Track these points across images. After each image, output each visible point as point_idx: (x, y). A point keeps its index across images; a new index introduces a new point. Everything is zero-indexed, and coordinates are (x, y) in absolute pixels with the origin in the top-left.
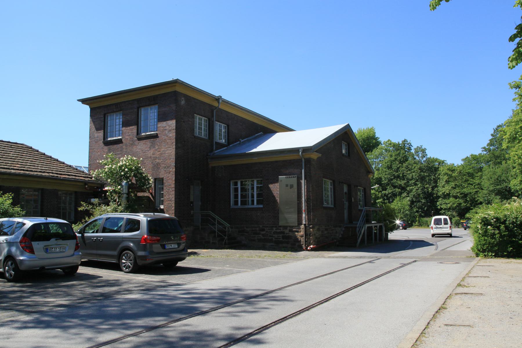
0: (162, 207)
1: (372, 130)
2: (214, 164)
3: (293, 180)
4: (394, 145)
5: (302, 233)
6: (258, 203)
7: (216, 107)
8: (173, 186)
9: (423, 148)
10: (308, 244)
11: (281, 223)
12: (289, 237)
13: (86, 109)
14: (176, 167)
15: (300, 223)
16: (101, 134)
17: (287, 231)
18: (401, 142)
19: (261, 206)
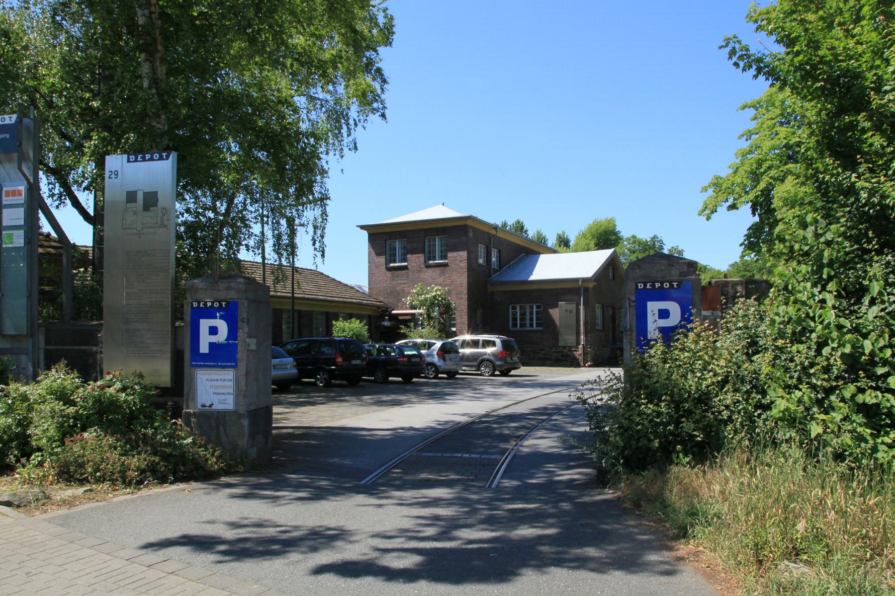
0: (454, 329)
1: (611, 221)
2: (491, 289)
3: (573, 307)
4: (640, 243)
5: (580, 351)
6: (537, 325)
7: (493, 236)
8: (466, 311)
9: (680, 249)
10: (585, 361)
11: (560, 344)
12: (568, 356)
13: (365, 234)
14: (468, 294)
15: (578, 343)
16: (382, 259)
17: (566, 351)
18: (649, 239)
19: (541, 328)
